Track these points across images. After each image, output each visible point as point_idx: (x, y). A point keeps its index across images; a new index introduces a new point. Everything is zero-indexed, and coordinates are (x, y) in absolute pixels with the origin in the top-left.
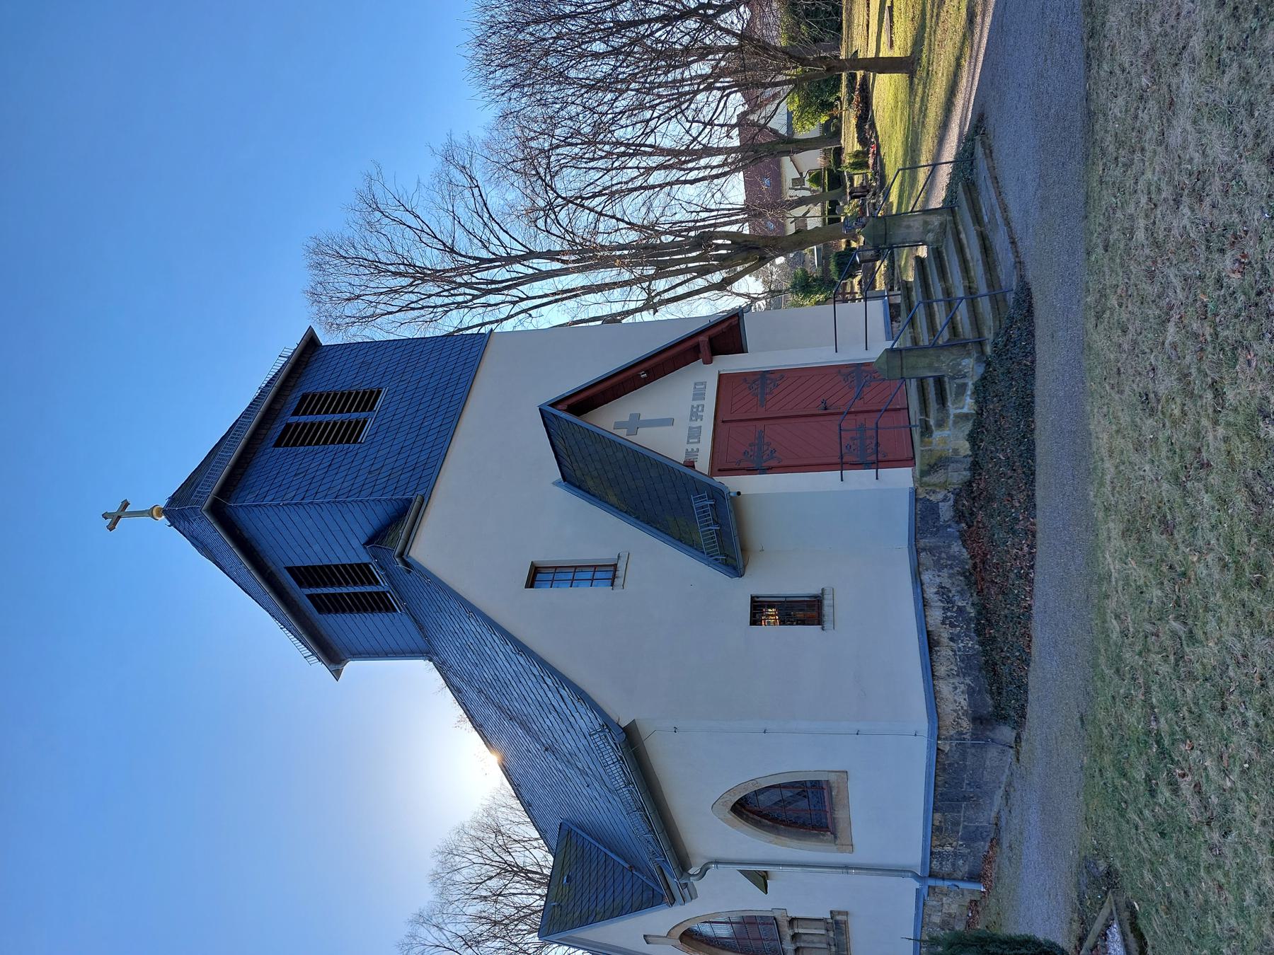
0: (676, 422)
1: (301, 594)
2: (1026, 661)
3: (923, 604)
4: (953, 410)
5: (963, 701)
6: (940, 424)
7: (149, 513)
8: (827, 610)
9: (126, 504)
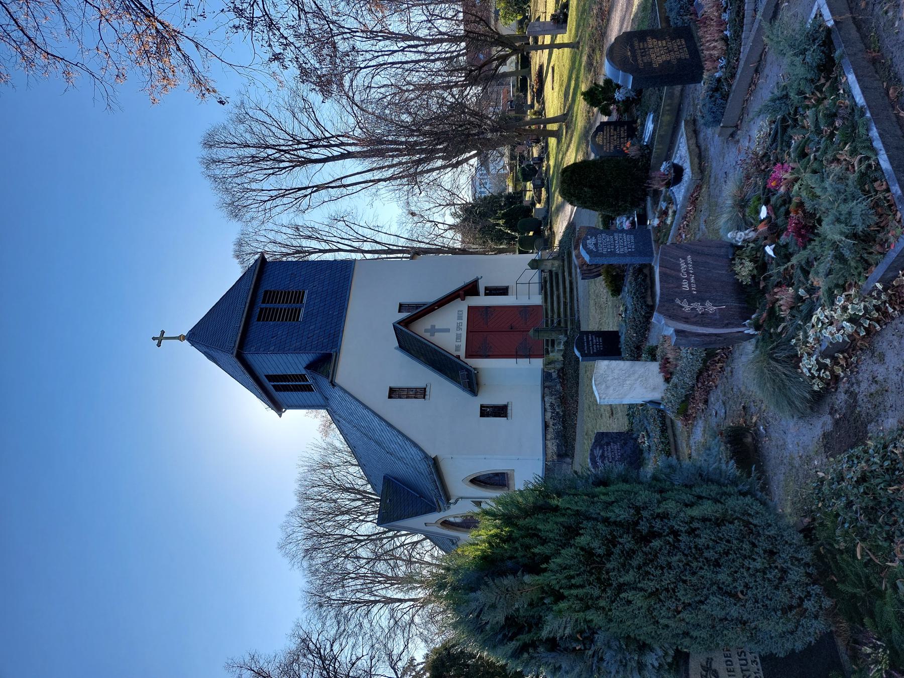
0: (449, 331)
1: (269, 385)
2: (574, 440)
3: (545, 410)
4: (556, 348)
5: (555, 448)
6: (552, 352)
7: (181, 338)
8: (509, 411)
9: (163, 332)
